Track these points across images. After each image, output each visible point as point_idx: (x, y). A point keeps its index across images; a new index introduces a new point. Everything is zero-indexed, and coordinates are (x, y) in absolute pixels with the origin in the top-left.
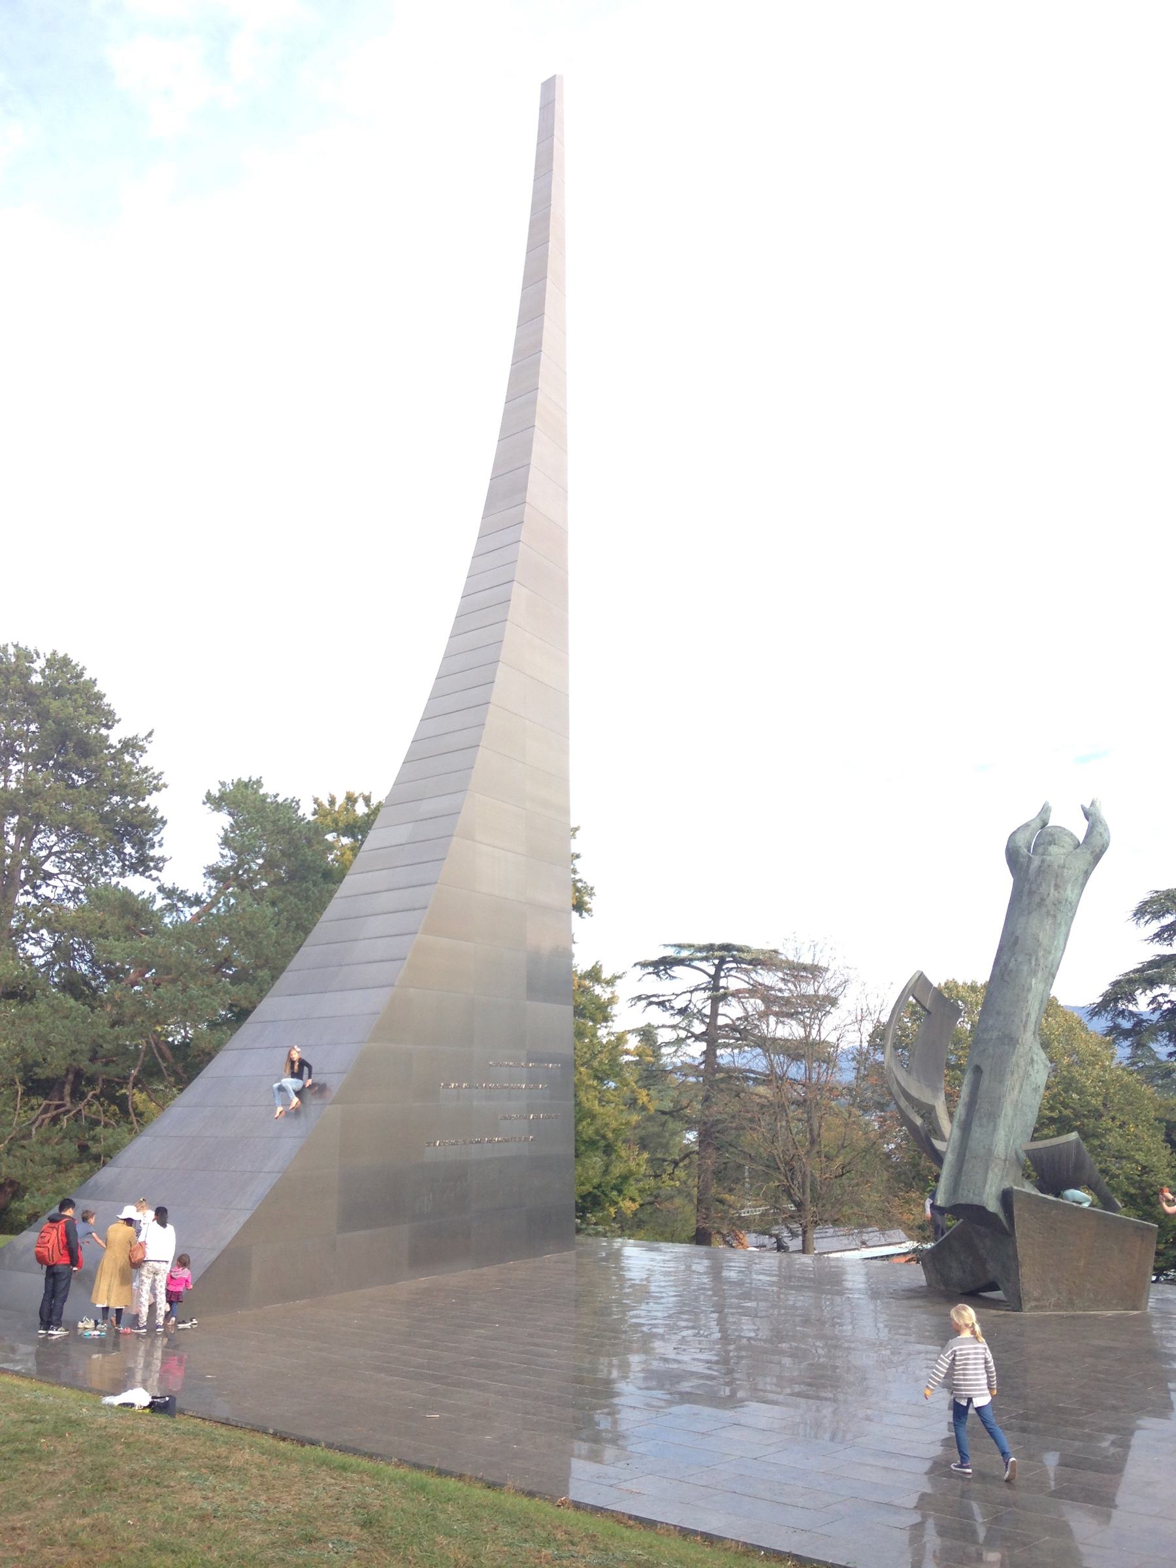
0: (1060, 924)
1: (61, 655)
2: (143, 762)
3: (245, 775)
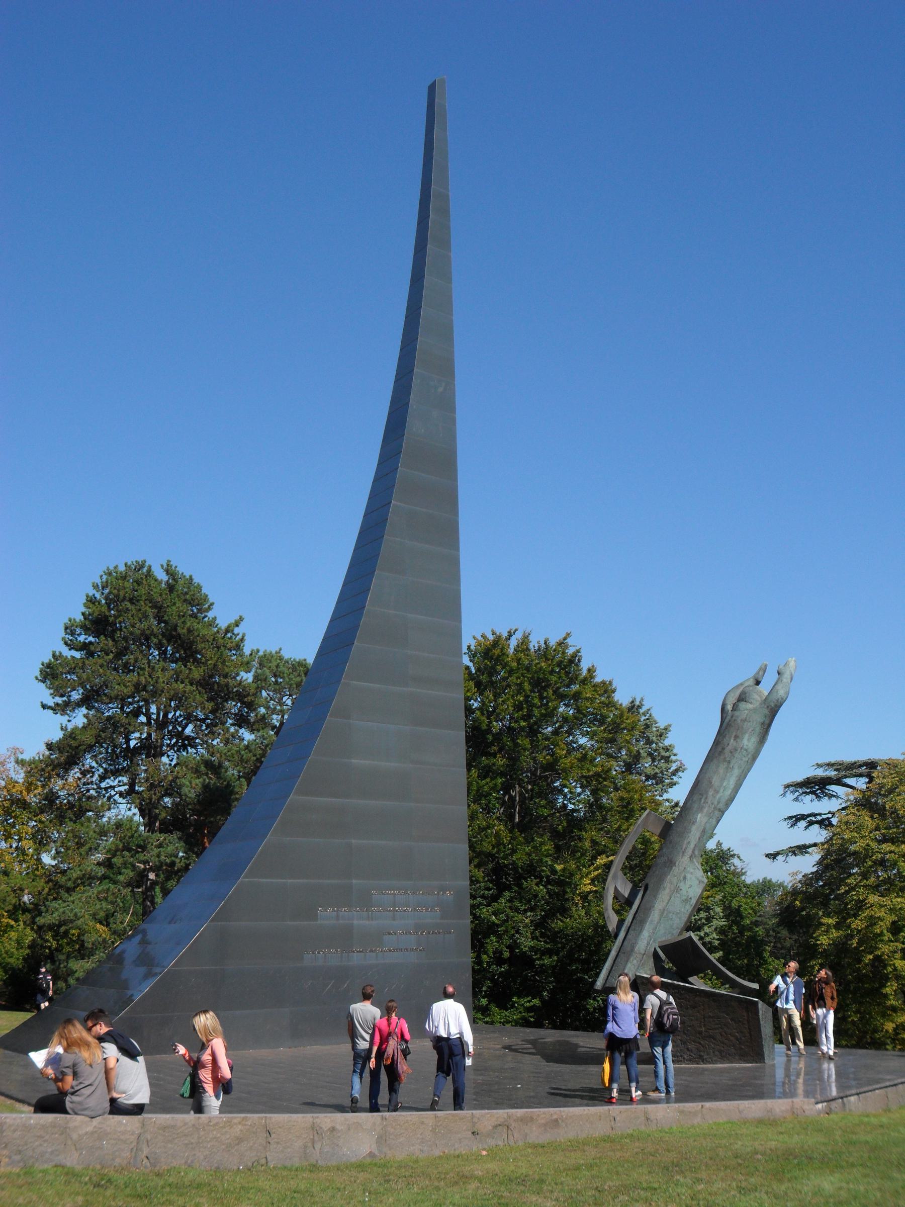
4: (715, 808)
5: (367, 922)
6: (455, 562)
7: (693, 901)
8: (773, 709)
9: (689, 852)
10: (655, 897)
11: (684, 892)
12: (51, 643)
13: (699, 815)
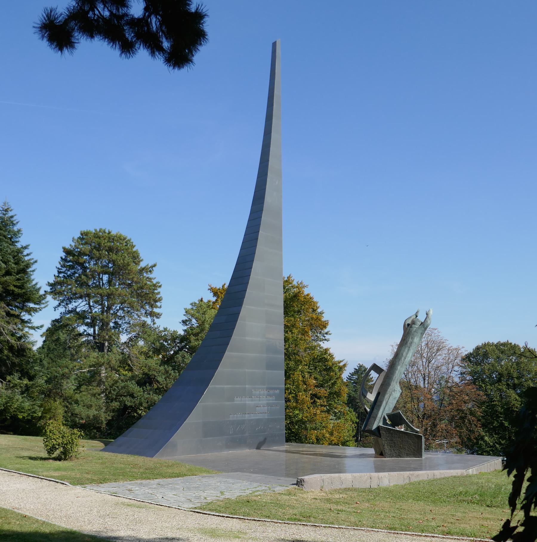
6: (281, 256)
7: (397, 399)
10: (384, 397)
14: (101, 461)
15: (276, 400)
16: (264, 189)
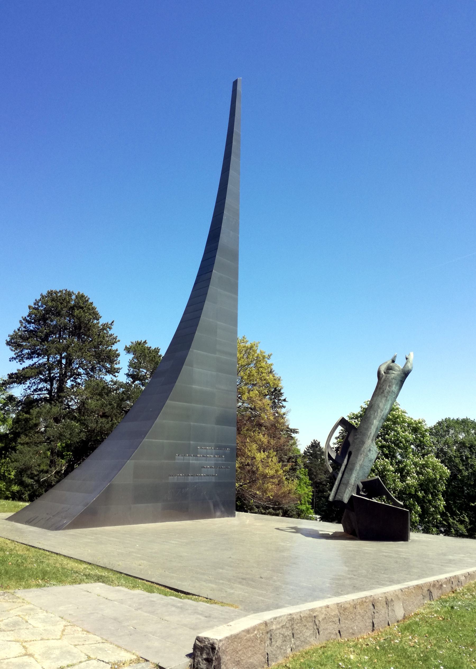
0: (389, 400)
1: (81, 293)
2: (110, 332)
3: (141, 339)
4: (382, 418)
5: (195, 462)
6: (236, 300)
8: (406, 374)
9: (371, 437)
10: (357, 457)
11: (369, 457)
12: (13, 325)
13: (375, 421)
14: (426, 560)
15: (225, 461)
16: (220, 228)
